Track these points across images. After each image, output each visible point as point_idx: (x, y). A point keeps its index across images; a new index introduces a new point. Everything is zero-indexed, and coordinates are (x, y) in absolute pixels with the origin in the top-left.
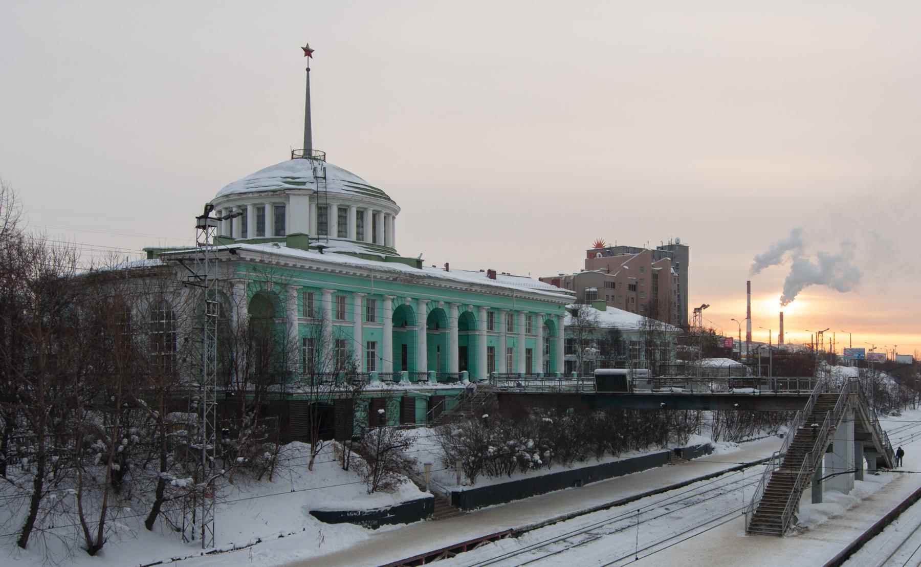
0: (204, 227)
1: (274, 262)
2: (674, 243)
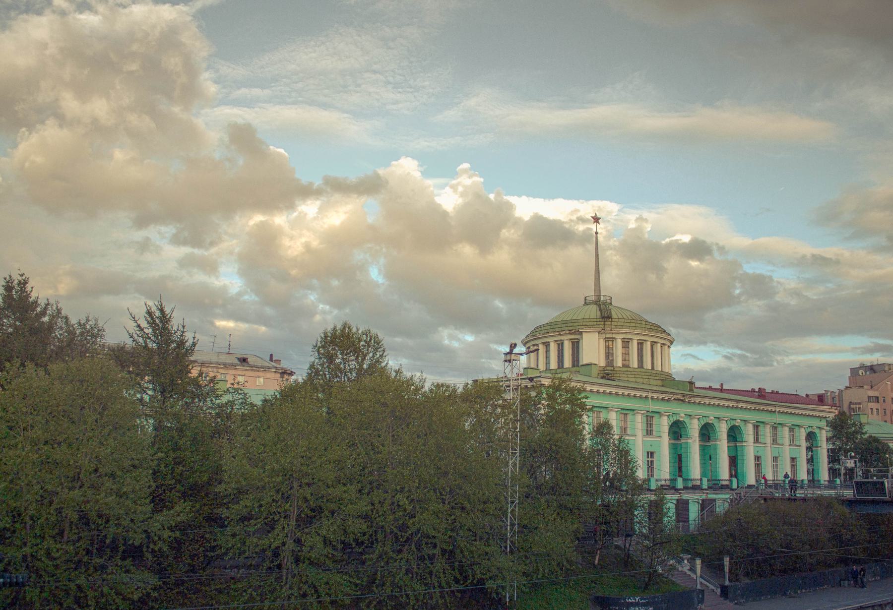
0: (510, 361)
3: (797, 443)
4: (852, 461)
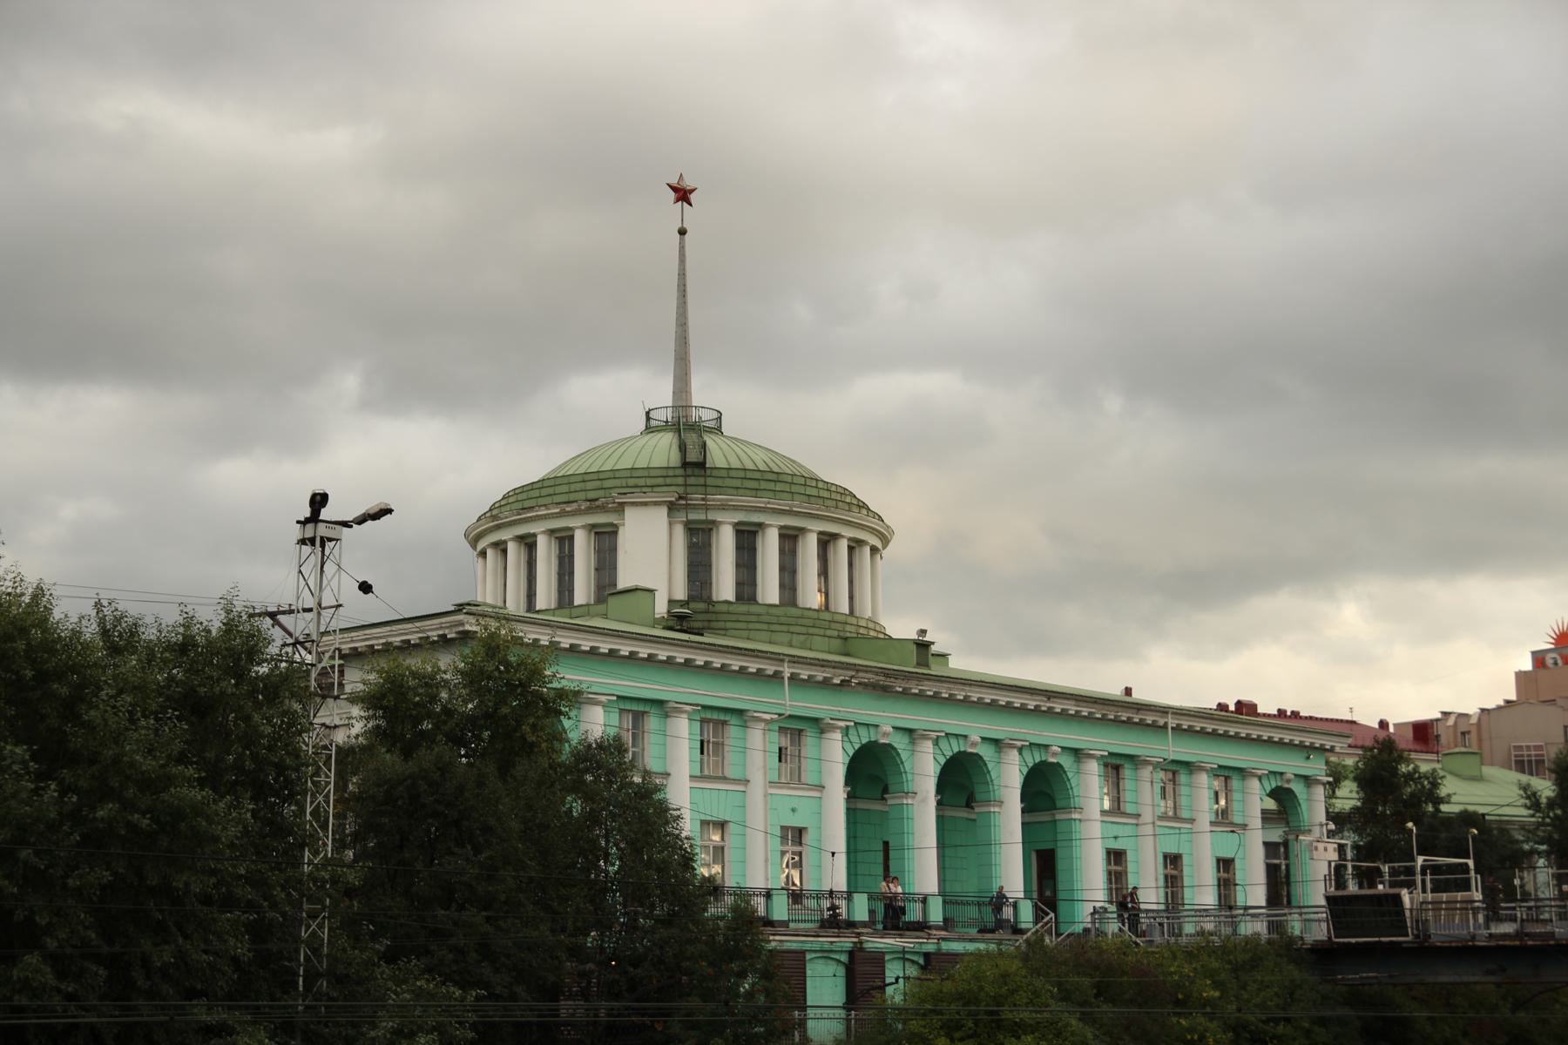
0: (312, 541)
1: (545, 641)
4: (1332, 847)
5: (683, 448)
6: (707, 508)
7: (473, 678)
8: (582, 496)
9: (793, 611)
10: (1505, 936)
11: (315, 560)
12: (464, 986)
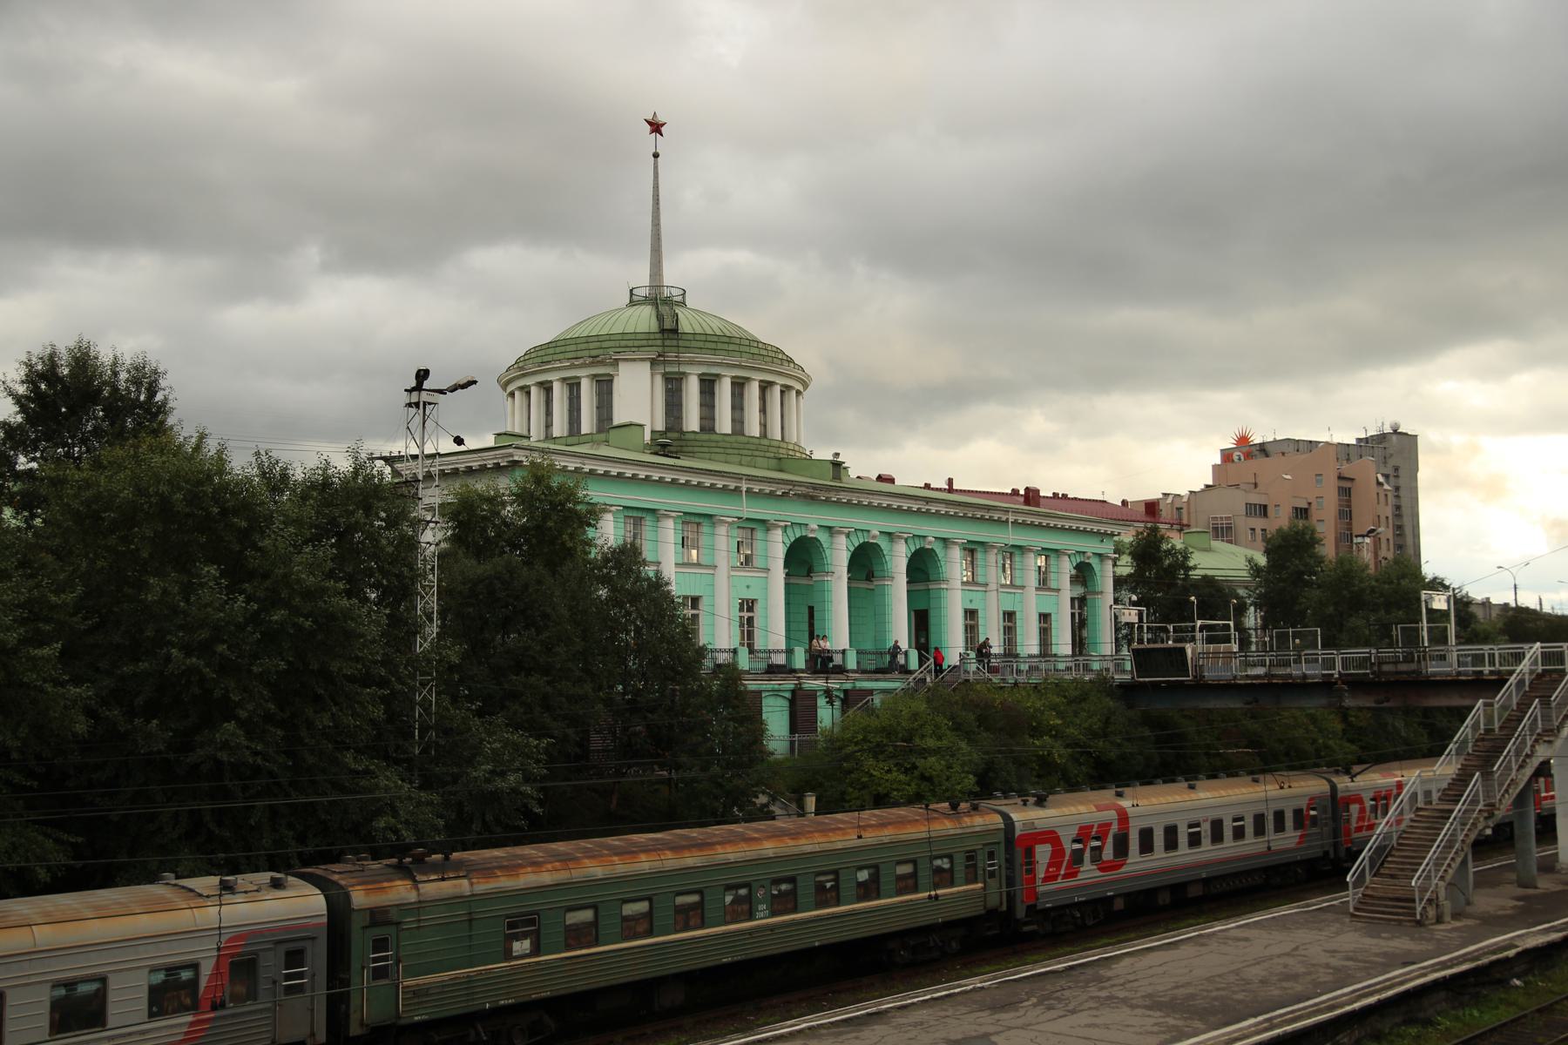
0: (417, 405)
2: (1388, 430)
3: (1053, 585)
4: (1134, 612)
5: (660, 318)
6: (679, 363)
7: (523, 497)
8: (586, 353)
9: (741, 439)
10: (1257, 677)
11: (418, 419)
12: (538, 737)
